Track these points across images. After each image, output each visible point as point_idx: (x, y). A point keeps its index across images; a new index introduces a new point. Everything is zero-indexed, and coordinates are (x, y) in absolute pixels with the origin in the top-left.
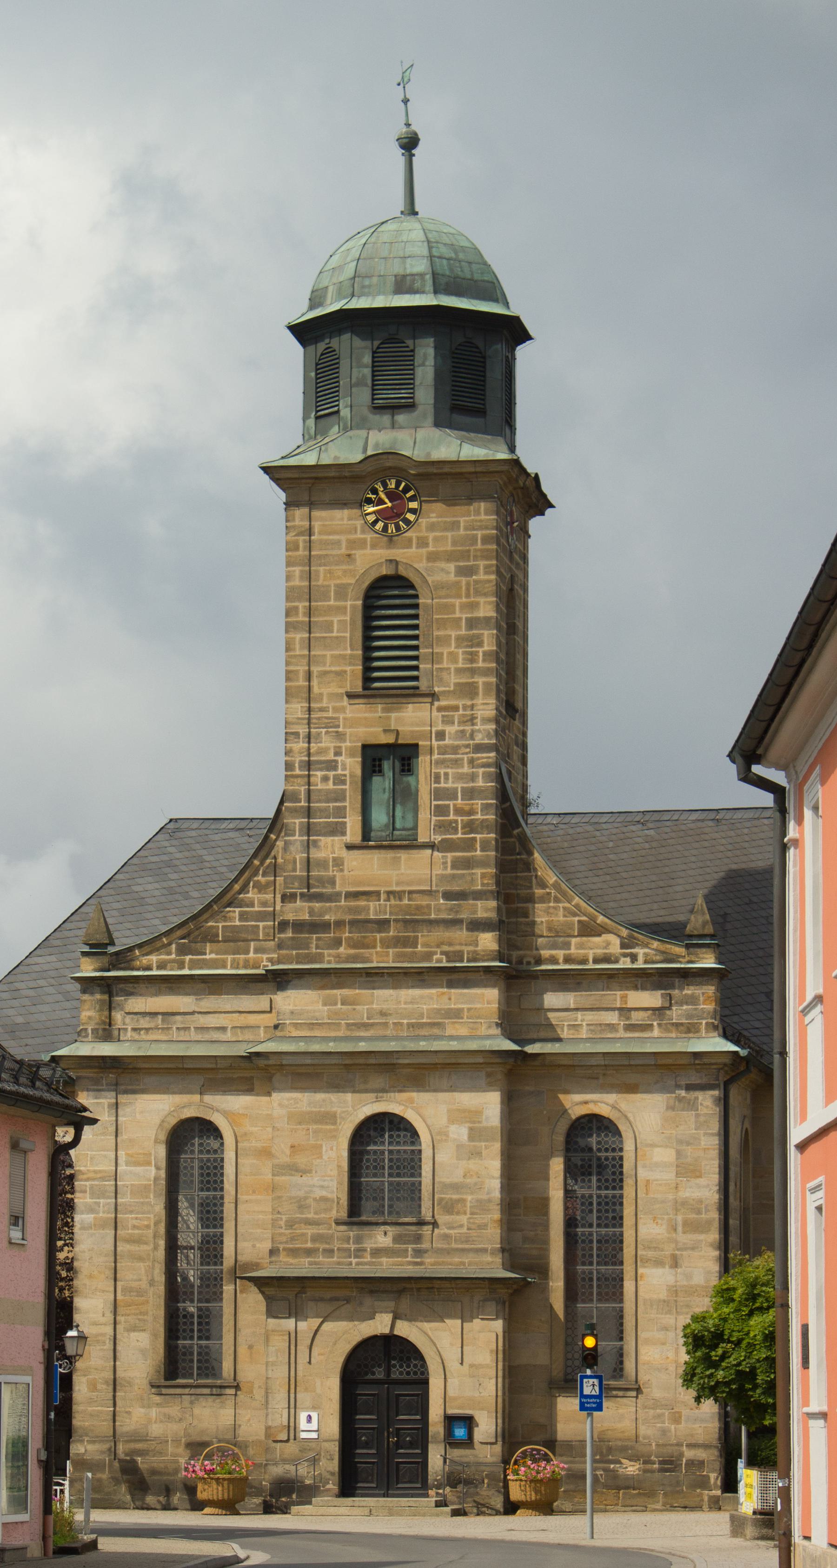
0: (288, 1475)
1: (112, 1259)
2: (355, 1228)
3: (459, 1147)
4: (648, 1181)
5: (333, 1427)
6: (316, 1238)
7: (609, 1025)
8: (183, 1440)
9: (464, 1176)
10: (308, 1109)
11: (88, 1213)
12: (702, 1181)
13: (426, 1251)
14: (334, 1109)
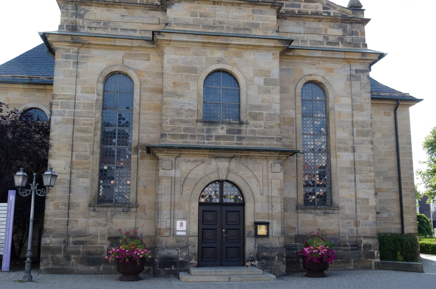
0: (170, 255)
1: (71, 140)
2: (207, 124)
3: (259, 87)
4: (340, 112)
5: (195, 229)
6: (186, 130)
7: (319, 41)
8: (106, 236)
9: (262, 102)
10: (183, 65)
11: (59, 116)
12: (365, 113)
13: (244, 138)
14: (196, 66)
